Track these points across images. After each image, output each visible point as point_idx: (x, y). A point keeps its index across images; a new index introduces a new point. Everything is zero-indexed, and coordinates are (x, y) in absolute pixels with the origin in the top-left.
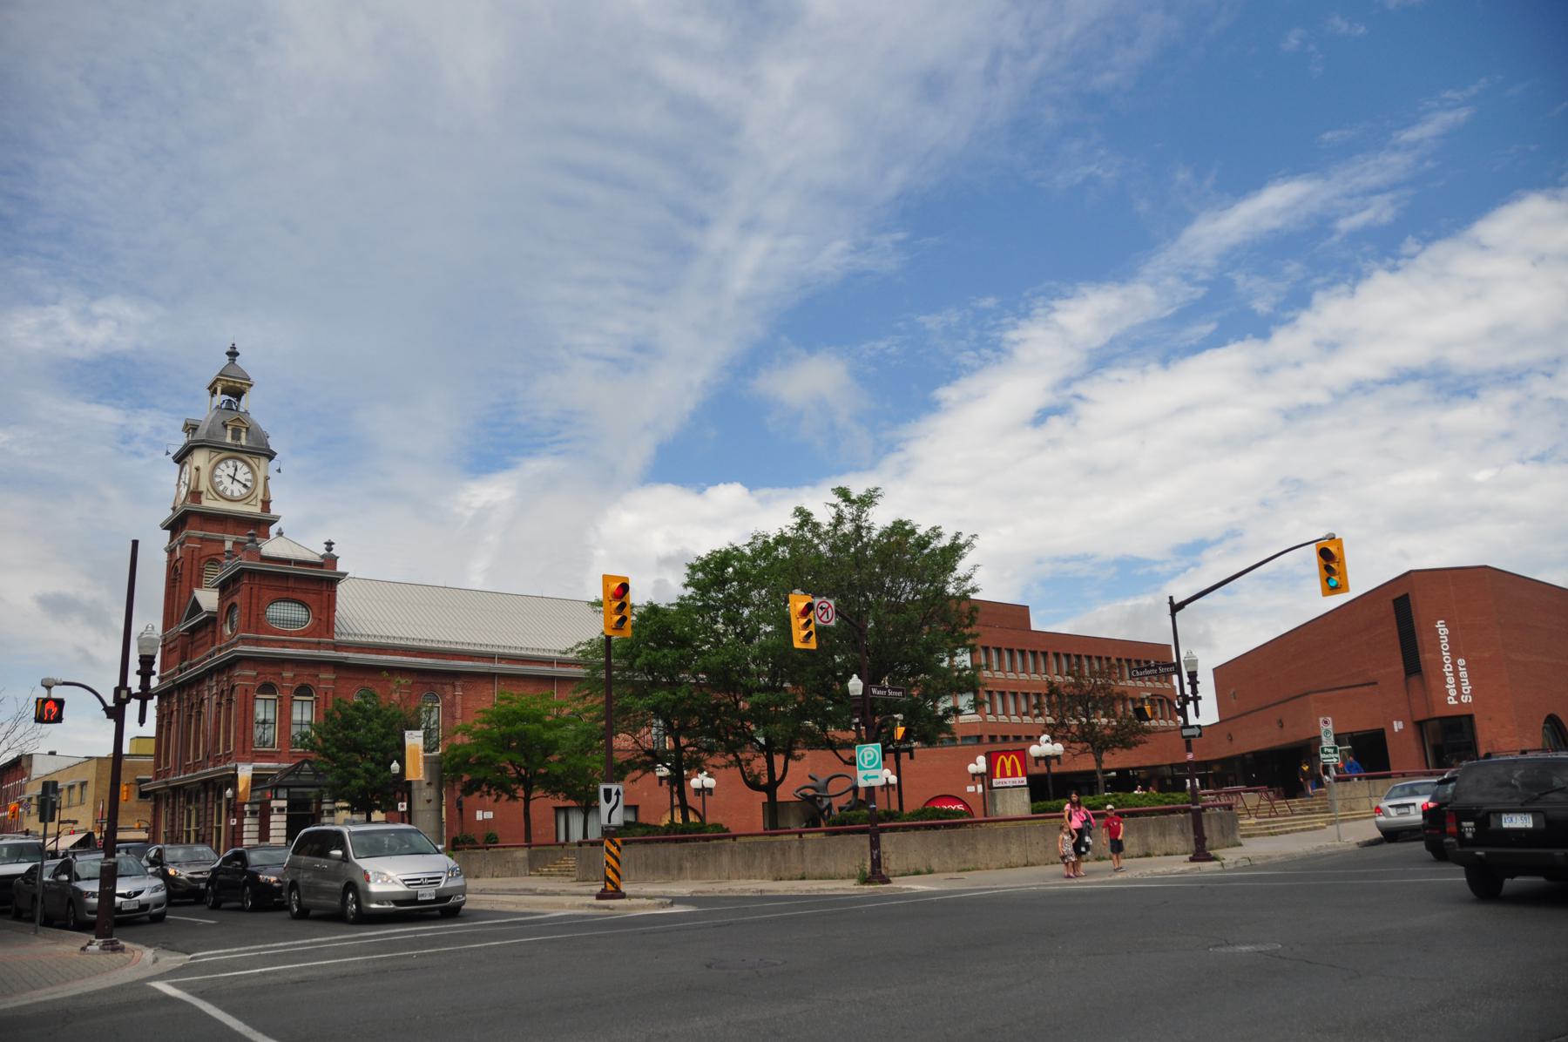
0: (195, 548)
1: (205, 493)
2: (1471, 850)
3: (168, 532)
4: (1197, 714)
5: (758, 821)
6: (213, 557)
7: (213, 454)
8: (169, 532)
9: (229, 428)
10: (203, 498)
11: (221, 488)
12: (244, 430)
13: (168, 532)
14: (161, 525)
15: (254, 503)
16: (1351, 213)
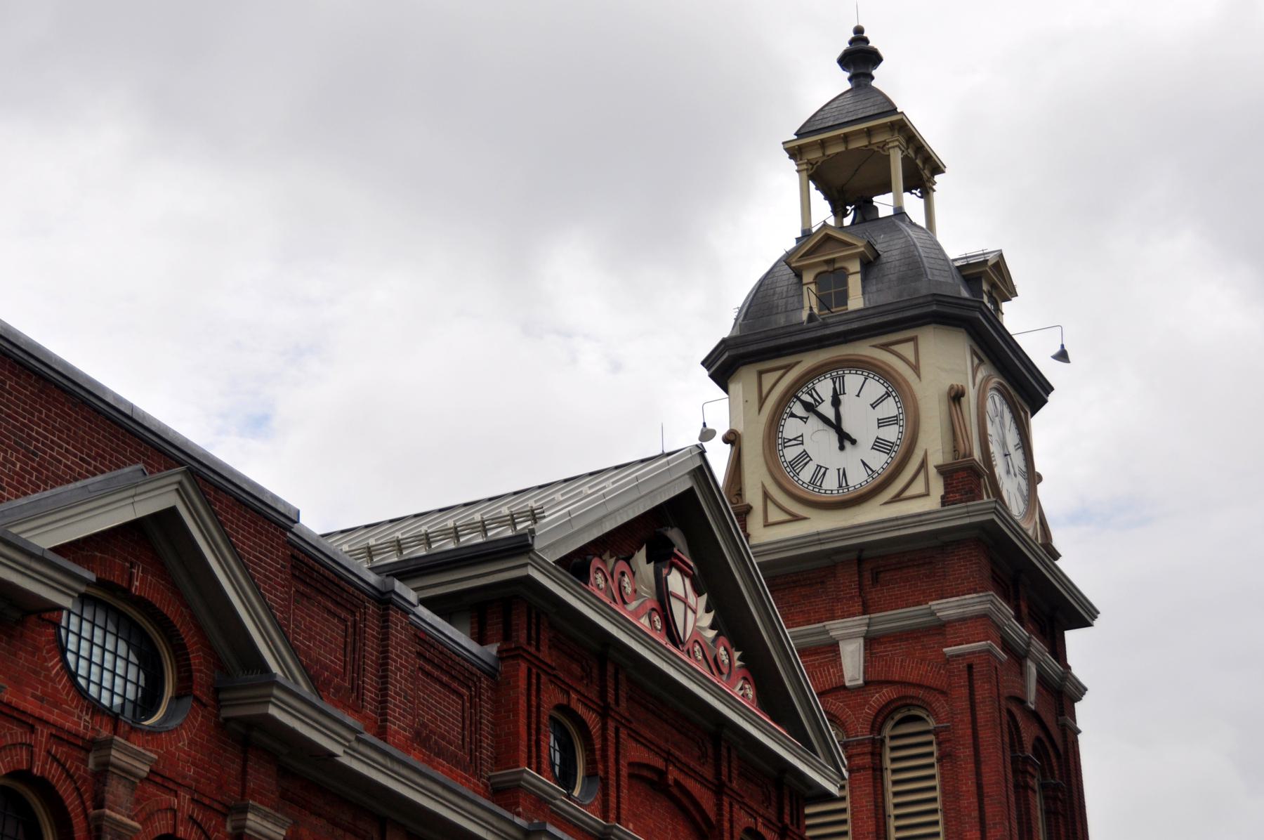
11: (806, 475)
12: (855, 266)
15: (918, 487)
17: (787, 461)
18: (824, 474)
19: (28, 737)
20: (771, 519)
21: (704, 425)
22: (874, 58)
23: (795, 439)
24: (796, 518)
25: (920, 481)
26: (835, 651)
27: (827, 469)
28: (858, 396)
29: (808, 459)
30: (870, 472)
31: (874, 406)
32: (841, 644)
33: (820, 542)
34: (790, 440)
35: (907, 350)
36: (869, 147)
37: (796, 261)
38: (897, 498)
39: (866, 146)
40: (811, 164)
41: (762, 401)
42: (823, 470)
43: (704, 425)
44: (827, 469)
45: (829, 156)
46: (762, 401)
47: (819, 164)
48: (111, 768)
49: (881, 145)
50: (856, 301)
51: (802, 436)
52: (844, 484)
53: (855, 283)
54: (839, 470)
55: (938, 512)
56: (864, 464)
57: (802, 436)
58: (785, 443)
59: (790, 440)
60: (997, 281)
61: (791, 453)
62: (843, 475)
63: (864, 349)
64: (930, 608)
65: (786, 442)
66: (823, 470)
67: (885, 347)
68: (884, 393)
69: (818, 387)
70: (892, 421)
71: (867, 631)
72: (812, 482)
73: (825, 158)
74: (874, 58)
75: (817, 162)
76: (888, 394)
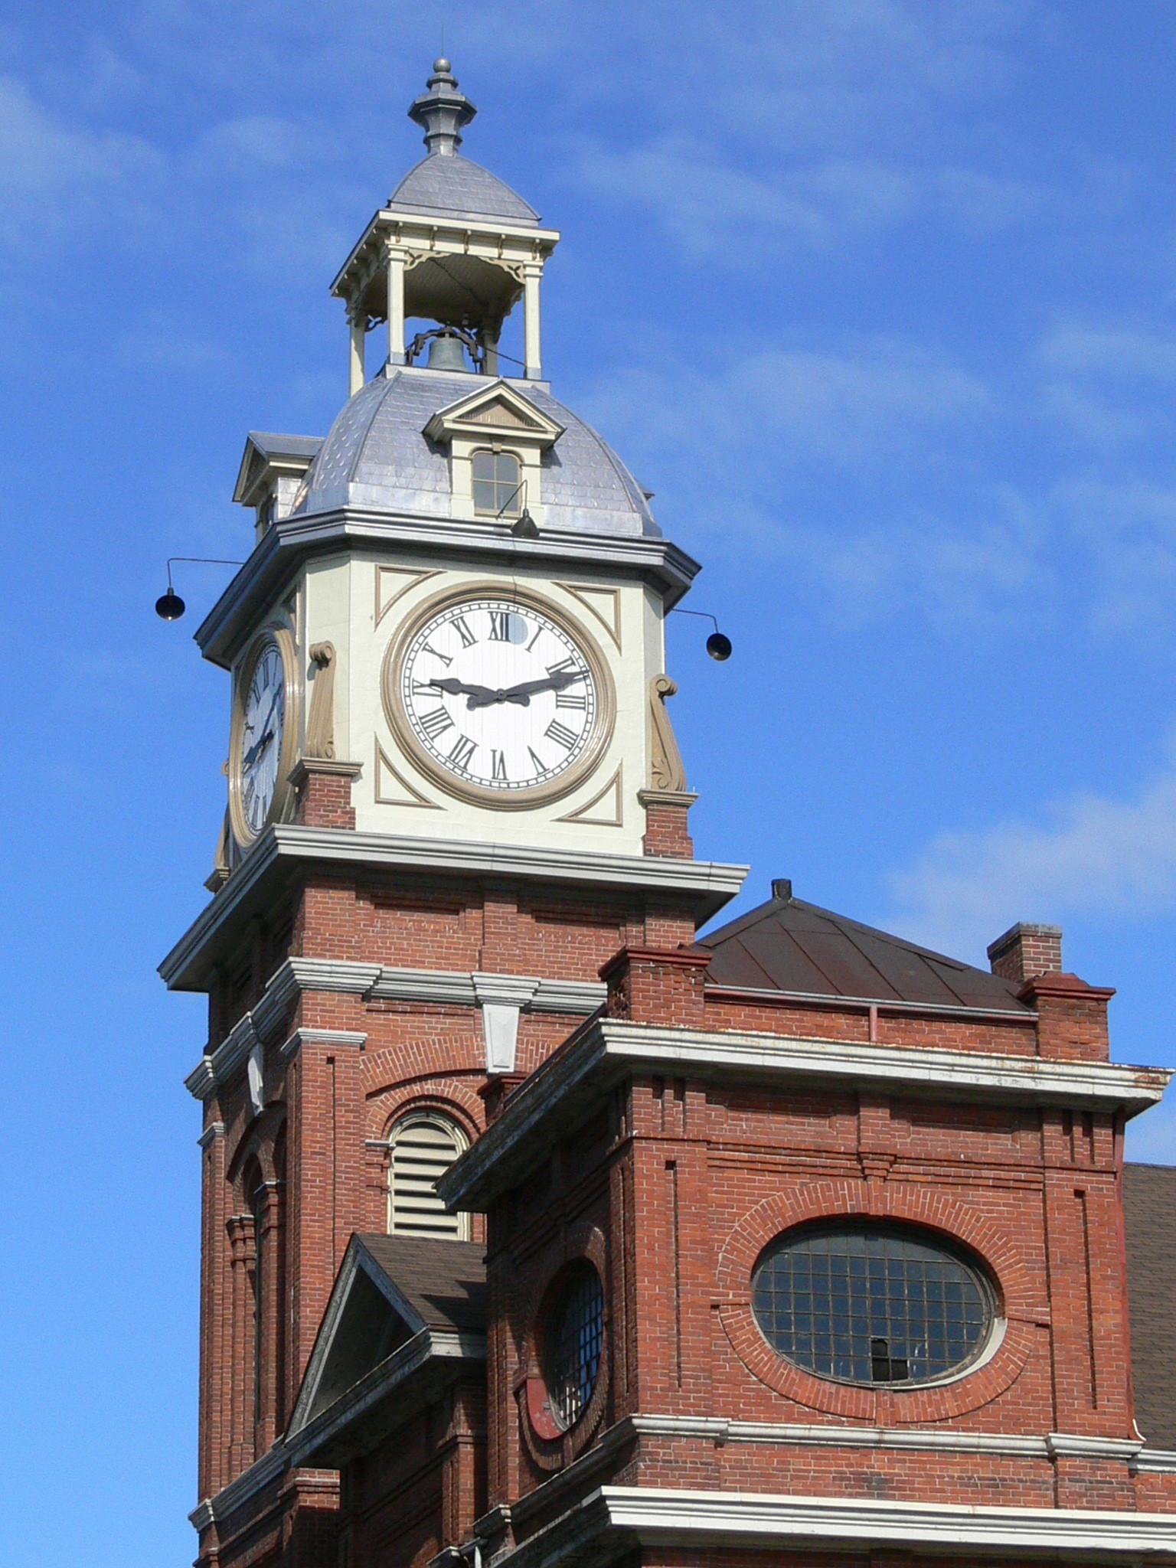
0: (340, 1045)
1: (367, 771)
2: (254, 1011)
3: (199, 1003)
4: (507, 1067)
5: (637, 968)
6: (430, 1087)
7: (394, 582)
8: (204, 998)
9: (460, 447)
10: (360, 794)
11: (444, 744)
12: (532, 455)
13: (199, 1003)
14: (166, 970)
15: (605, 809)
16: (938, 1047)
17: (417, 715)
18: (471, 752)
19: (239, 781)
20: (383, 796)
24: (424, 803)
25: (608, 803)
27: (475, 745)
29: (554, 724)
30: (541, 770)
35: (603, 603)
36: (496, 262)
37: (454, 421)
38: (574, 818)
40: (411, 255)
42: (469, 745)
44: (475, 745)
45: (439, 252)
47: (423, 259)
48: (279, 841)
52: (501, 776)
54: (494, 752)
56: (533, 755)
58: (414, 687)
60: (255, 486)
63: (542, 586)
66: (469, 745)
67: (571, 590)
68: (568, 657)
71: (372, 987)
72: (452, 758)
75: (419, 257)
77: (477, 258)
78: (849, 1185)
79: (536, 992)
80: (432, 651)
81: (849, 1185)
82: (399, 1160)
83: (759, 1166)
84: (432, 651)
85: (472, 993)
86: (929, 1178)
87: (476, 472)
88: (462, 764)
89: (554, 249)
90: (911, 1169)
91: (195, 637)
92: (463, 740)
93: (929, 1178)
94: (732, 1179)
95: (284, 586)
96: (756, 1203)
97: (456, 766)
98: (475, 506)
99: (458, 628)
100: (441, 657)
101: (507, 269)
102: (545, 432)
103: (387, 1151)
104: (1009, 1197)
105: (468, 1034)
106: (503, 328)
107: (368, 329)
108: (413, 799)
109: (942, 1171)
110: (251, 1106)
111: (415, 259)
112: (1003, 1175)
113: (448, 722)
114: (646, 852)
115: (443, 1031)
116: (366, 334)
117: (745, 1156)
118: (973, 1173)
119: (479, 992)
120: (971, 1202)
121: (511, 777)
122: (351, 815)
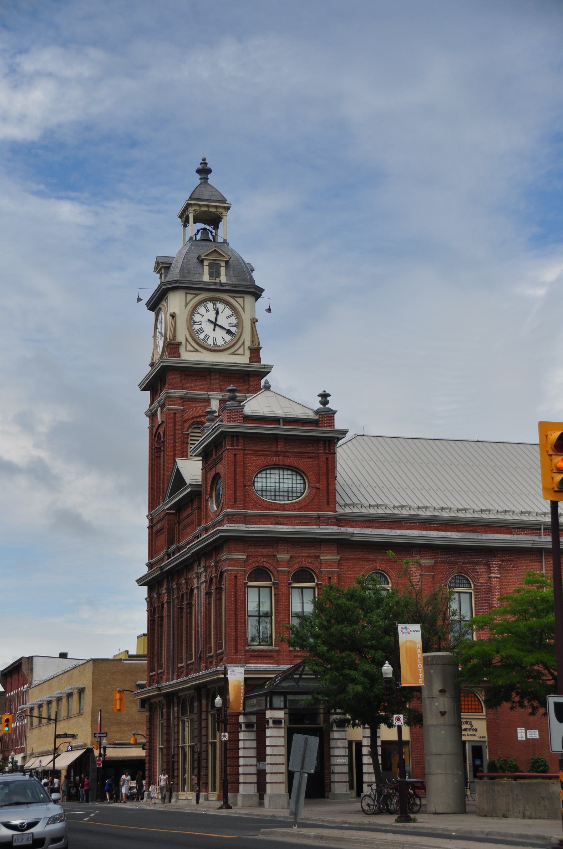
0: (176, 410)
3: (148, 393)
6: (198, 419)
8: (149, 392)
9: (206, 263)
10: (182, 350)
11: (202, 336)
12: (223, 264)
13: (148, 393)
15: (240, 351)
18: (208, 338)
20: (188, 349)
21: (139, 296)
22: (209, 171)
23: (198, 322)
24: (197, 351)
25: (241, 349)
26: (208, 402)
27: (209, 336)
28: (222, 312)
31: (228, 318)
32: (211, 400)
33: (213, 365)
34: (196, 322)
35: (240, 300)
36: (216, 212)
37: (204, 256)
38: (233, 353)
39: (215, 211)
41: (187, 305)
42: (208, 336)
43: (139, 296)
44: (209, 336)
46: (187, 305)
47: (198, 212)
49: (220, 213)
50: (223, 279)
51: (201, 322)
52: (215, 344)
53: (223, 270)
54: (214, 338)
55: (248, 364)
57: (201, 322)
59: (196, 322)
61: (197, 327)
62: (215, 340)
63: (226, 297)
64: (246, 395)
65: (195, 322)
66: (208, 336)
67: (233, 297)
69: (208, 305)
70: (234, 325)
73: (200, 211)
74: (209, 171)
76: (233, 315)
77: (211, 211)
78: (275, 458)
79: (223, 396)
80: (199, 314)
81: (275, 458)
82: (191, 436)
83: (255, 454)
84: (199, 314)
85: (208, 397)
86: (293, 456)
87: (209, 269)
88: (206, 341)
89: (230, 208)
90: (289, 454)
91: (146, 304)
92: (206, 335)
93: (293, 456)
94: (249, 457)
95: (164, 297)
96: (254, 462)
97: (205, 342)
98: (210, 277)
99: (205, 308)
100: (201, 315)
101: (219, 214)
102: (226, 258)
103: (189, 434)
104: (311, 460)
105: (207, 406)
106: (219, 226)
107: (186, 227)
108: (194, 350)
109: (296, 454)
110: (159, 422)
111: (196, 212)
112: (310, 455)
113: (203, 331)
114: (250, 362)
115: (201, 406)
116: (186, 228)
117: (252, 452)
118: (303, 455)
119: (210, 396)
120: (303, 461)
121: (218, 344)
122: (180, 354)
